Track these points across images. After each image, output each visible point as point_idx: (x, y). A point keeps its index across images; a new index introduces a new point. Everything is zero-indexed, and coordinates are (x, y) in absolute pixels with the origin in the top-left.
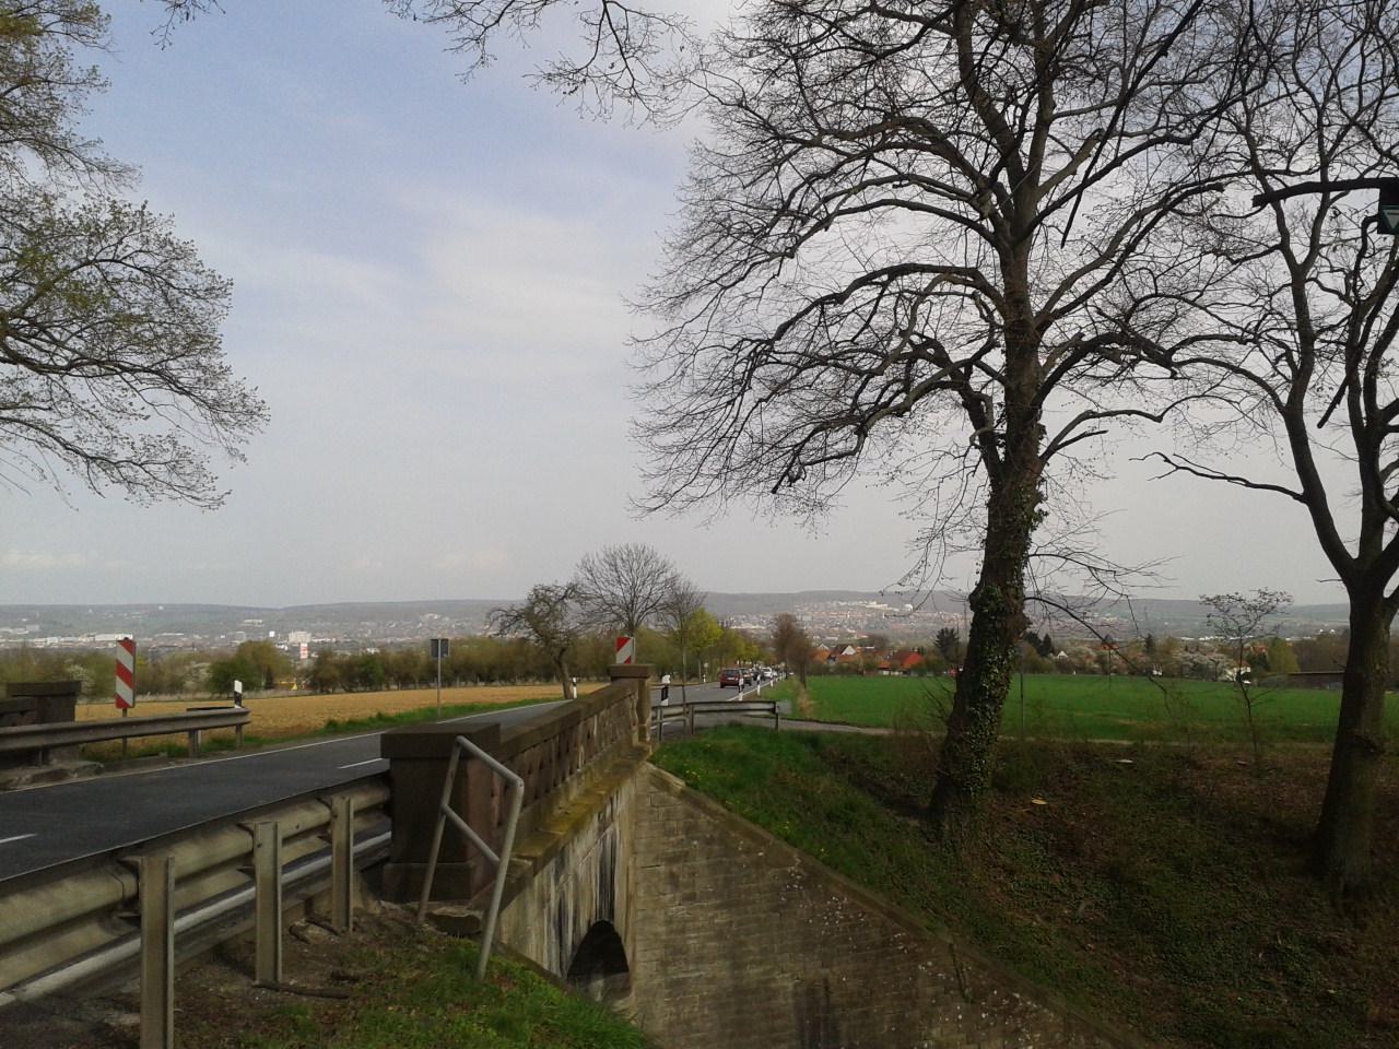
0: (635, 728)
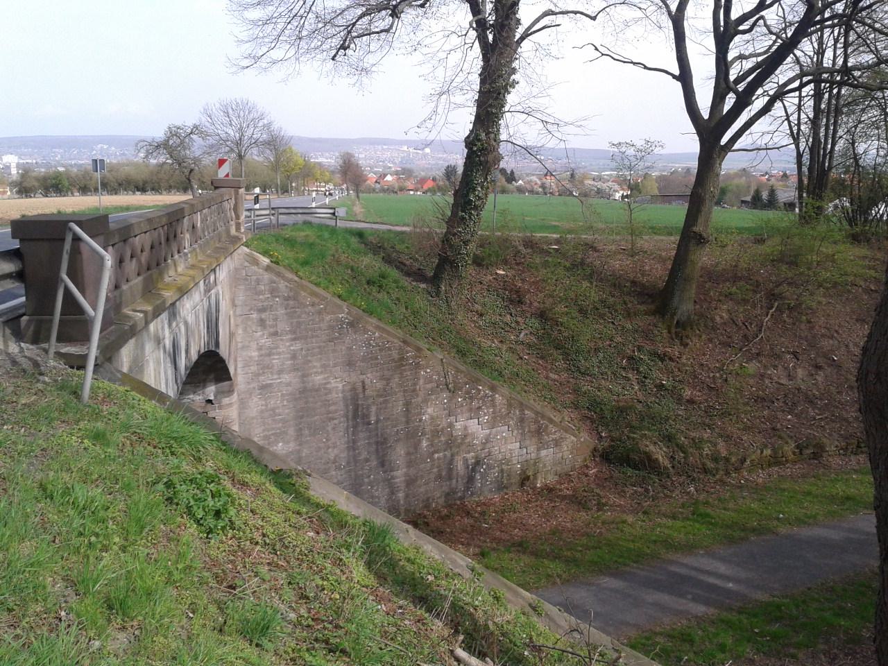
0: (232, 223)
